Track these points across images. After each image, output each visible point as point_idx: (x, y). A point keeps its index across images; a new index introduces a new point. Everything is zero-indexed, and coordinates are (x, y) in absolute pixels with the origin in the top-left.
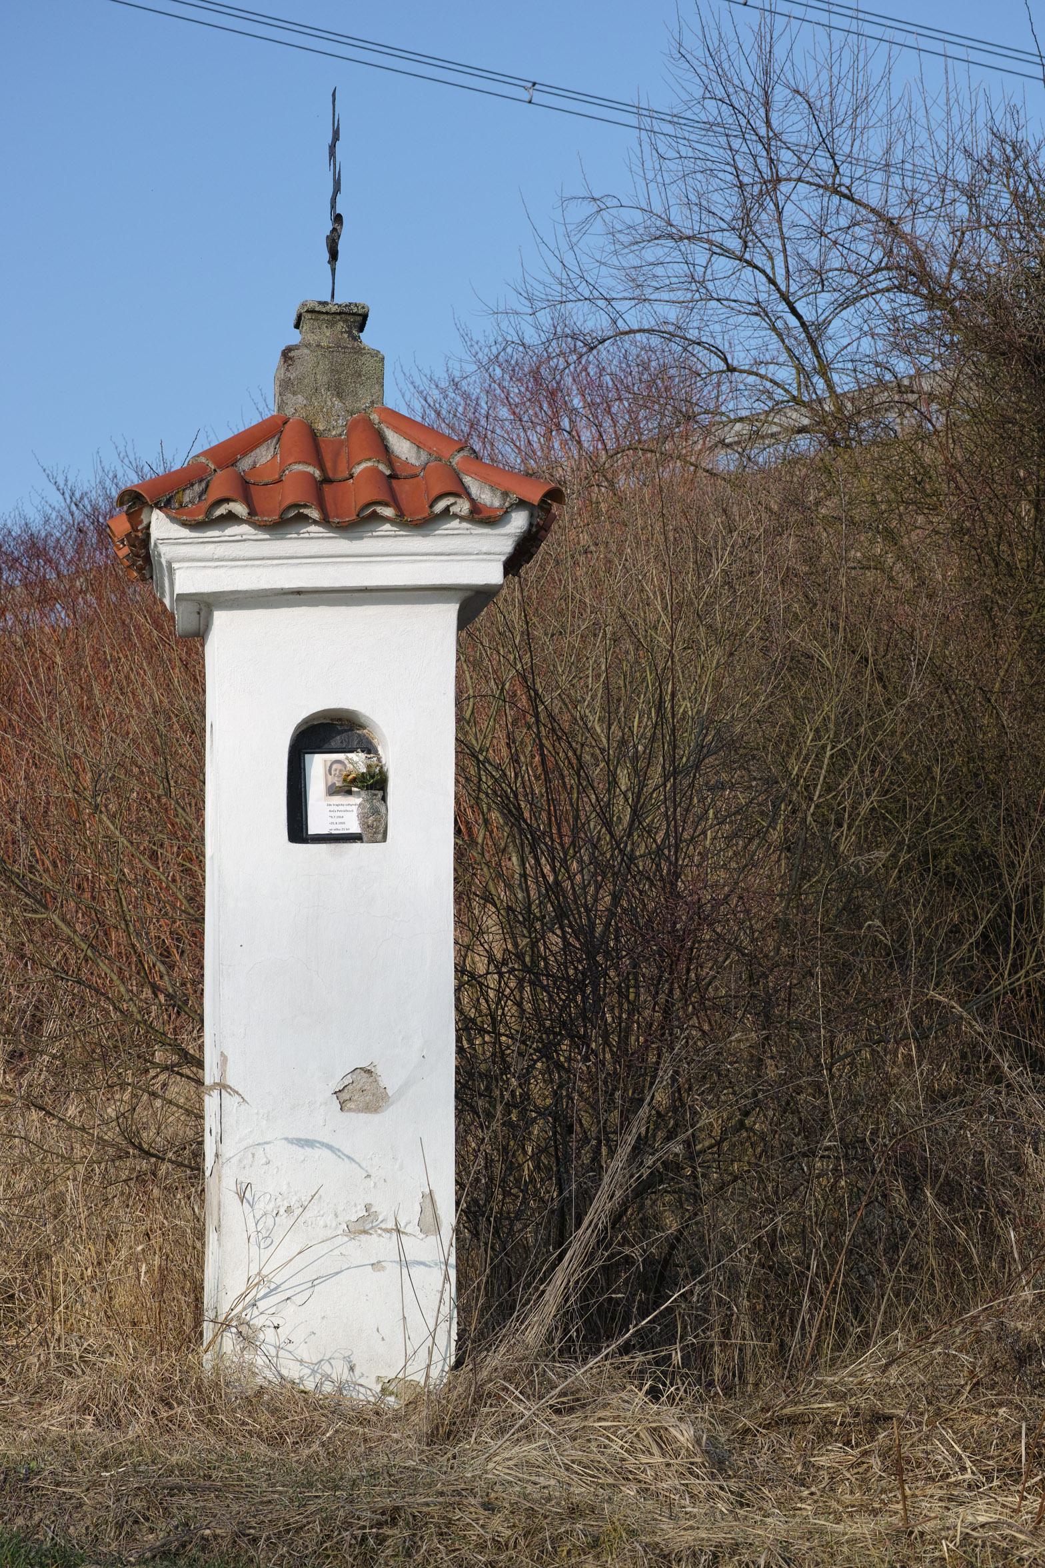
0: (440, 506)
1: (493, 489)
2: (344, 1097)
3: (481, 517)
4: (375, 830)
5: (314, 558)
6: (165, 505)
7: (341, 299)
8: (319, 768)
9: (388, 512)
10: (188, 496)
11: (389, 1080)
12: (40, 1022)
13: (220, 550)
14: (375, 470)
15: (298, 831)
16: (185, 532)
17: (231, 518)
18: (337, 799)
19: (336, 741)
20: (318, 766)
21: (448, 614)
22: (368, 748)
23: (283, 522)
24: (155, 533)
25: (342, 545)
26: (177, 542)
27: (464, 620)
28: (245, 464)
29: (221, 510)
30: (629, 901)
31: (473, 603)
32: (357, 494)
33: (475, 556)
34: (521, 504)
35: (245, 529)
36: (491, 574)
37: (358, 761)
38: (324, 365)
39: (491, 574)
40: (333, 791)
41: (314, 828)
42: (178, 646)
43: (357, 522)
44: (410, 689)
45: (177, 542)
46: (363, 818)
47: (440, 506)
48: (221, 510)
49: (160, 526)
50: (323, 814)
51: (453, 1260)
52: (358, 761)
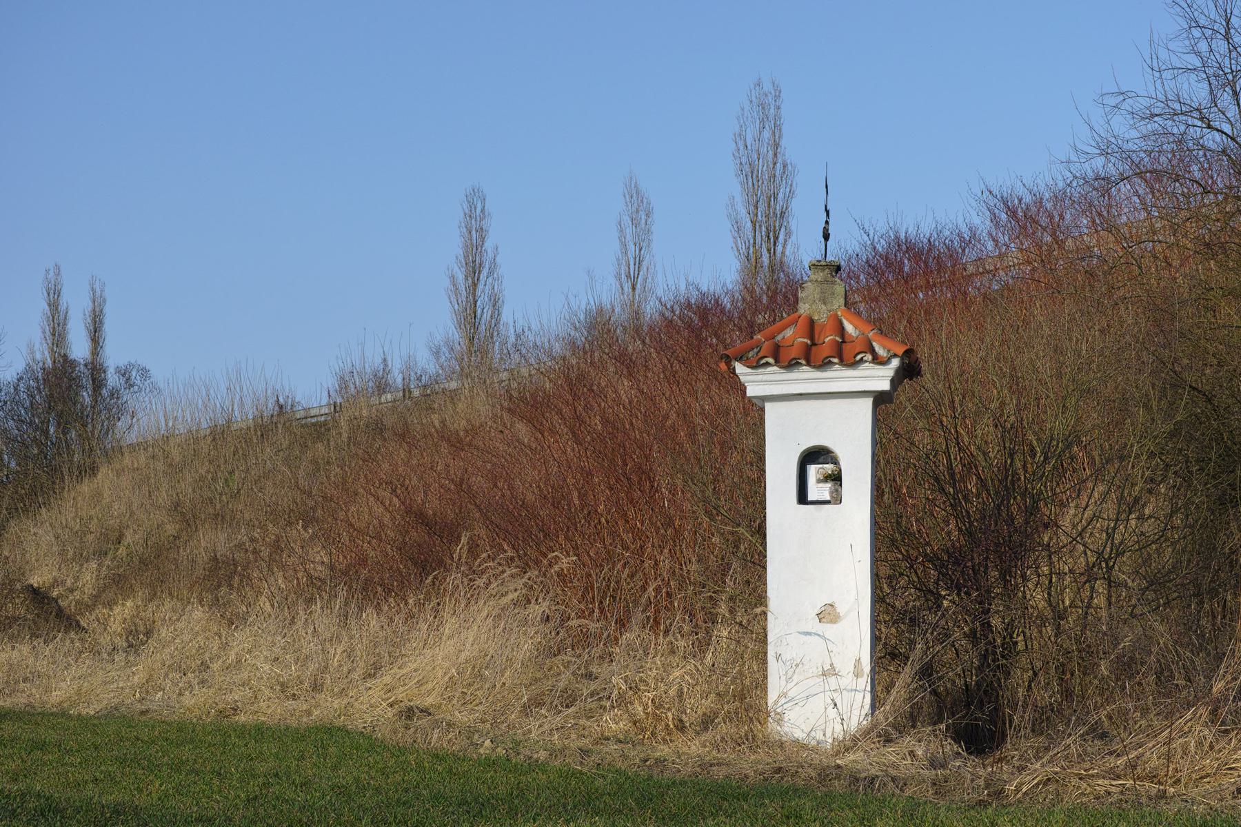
0: (859, 357)
1: (884, 348)
2: (821, 617)
3: (877, 360)
4: (836, 499)
5: (805, 379)
6: (740, 359)
7: (829, 258)
8: (813, 471)
9: (836, 360)
10: (750, 355)
11: (841, 609)
12: (911, 714)
13: (765, 378)
14: (834, 340)
15: (803, 498)
16: (749, 370)
17: (767, 364)
18: (821, 485)
19: (821, 459)
20: (813, 471)
21: (868, 403)
22: (835, 462)
23: (791, 365)
24: (737, 371)
25: (818, 374)
26: (746, 374)
27: (876, 405)
28: (779, 338)
29: (763, 361)
30: (1051, 539)
31: (880, 399)
32: (824, 351)
33: (879, 378)
34: (895, 356)
35: (775, 368)
36: (885, 386)
37: (829, 468)
38: (818, 290)
39: (885, 386)
40: (819, 481)
41: (811, 497)
42: (754, 412)
43: (824, 365)
44: (851, 434)
45: (746, 374)
46: (831, 493)
47: (859, 357)
48: (763, 361)
49: (740, 368)
50: (817, 490)
51: (869, 688)
52: (829, 468)
